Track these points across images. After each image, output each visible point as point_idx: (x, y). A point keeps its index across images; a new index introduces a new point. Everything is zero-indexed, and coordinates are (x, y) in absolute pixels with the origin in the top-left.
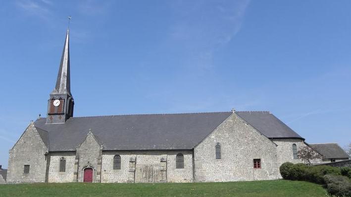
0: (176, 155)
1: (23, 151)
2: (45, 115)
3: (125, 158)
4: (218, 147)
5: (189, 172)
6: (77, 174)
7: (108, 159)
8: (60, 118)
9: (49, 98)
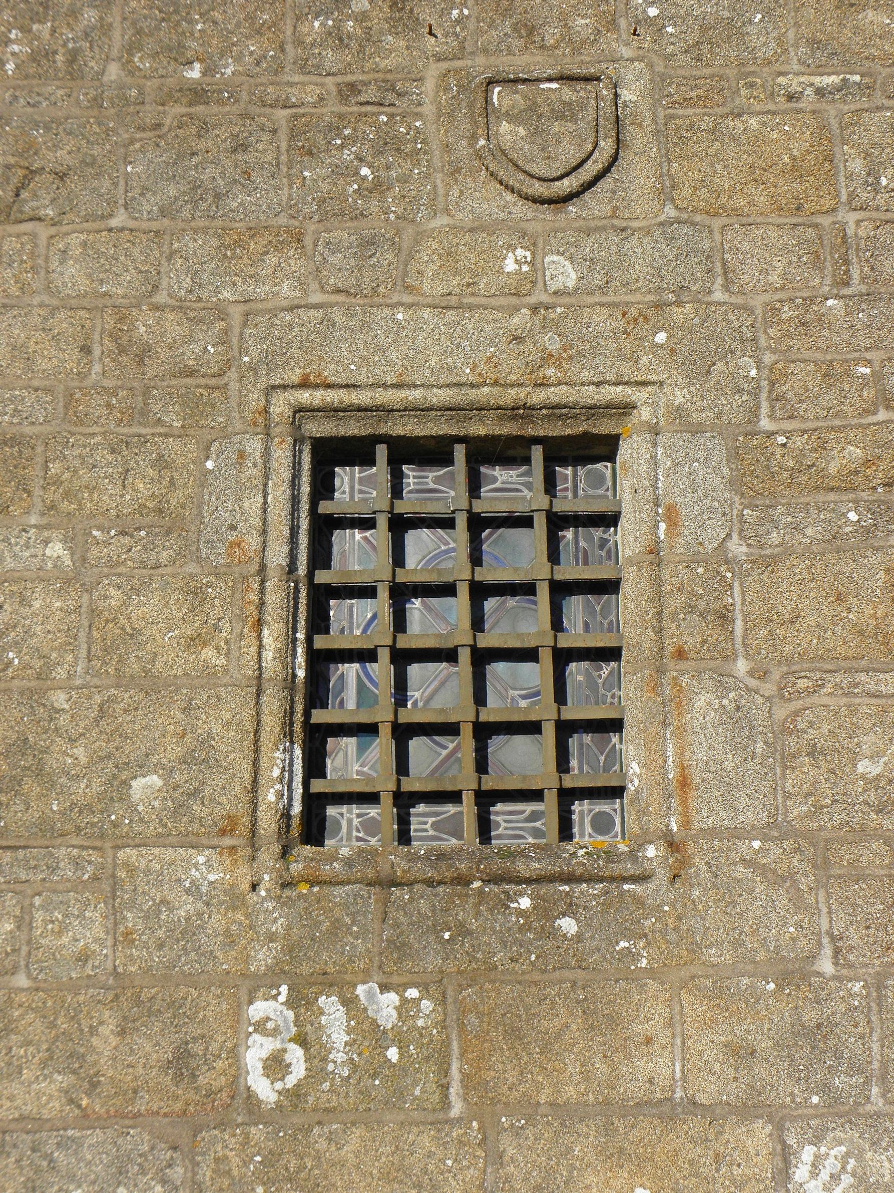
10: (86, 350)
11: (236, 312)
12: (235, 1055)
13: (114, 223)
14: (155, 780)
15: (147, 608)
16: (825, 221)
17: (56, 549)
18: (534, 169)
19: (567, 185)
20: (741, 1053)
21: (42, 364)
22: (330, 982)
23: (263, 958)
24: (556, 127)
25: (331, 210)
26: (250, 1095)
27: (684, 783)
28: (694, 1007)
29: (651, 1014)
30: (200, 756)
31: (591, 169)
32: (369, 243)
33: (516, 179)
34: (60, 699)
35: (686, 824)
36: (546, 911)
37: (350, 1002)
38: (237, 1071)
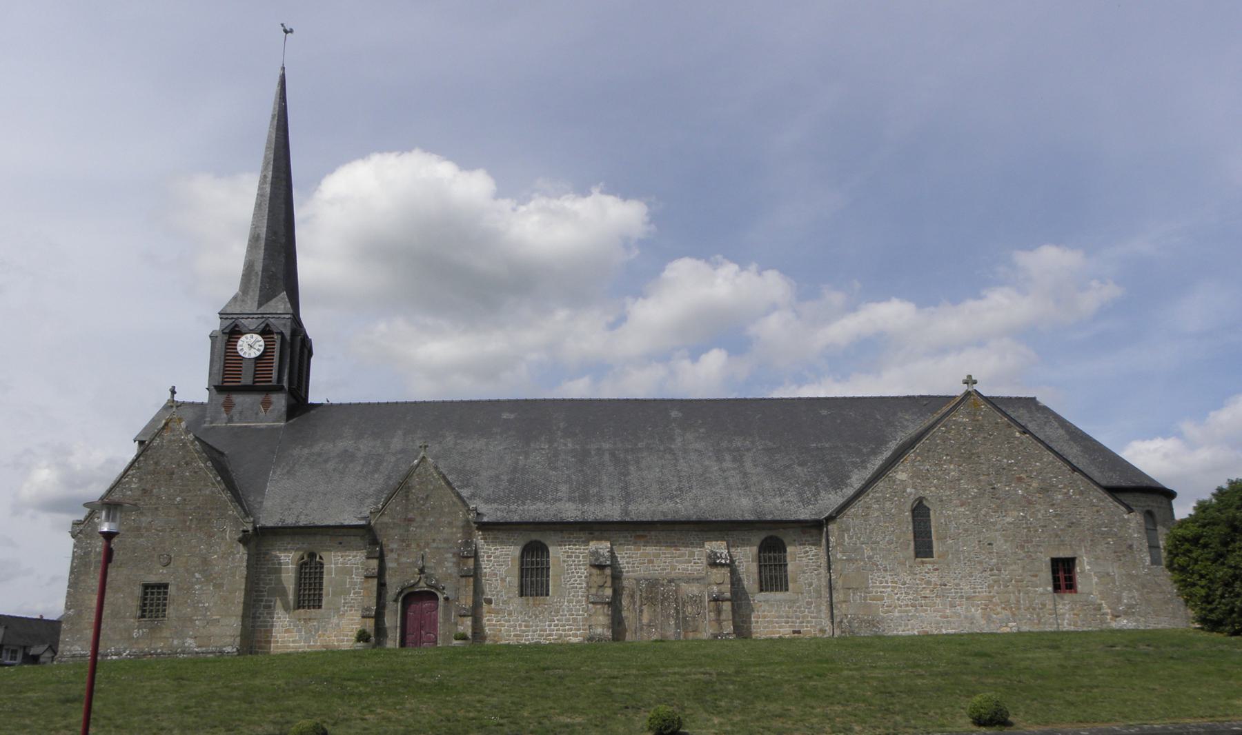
0: (755, 549)
1: (138, 529)
2: (196, 387)
3: (570, 562)
4: (920, 512)
5: (809, 603)
6: (379, 616)
7: (500, 561)
8: (266, 404)
9: (216, 325)
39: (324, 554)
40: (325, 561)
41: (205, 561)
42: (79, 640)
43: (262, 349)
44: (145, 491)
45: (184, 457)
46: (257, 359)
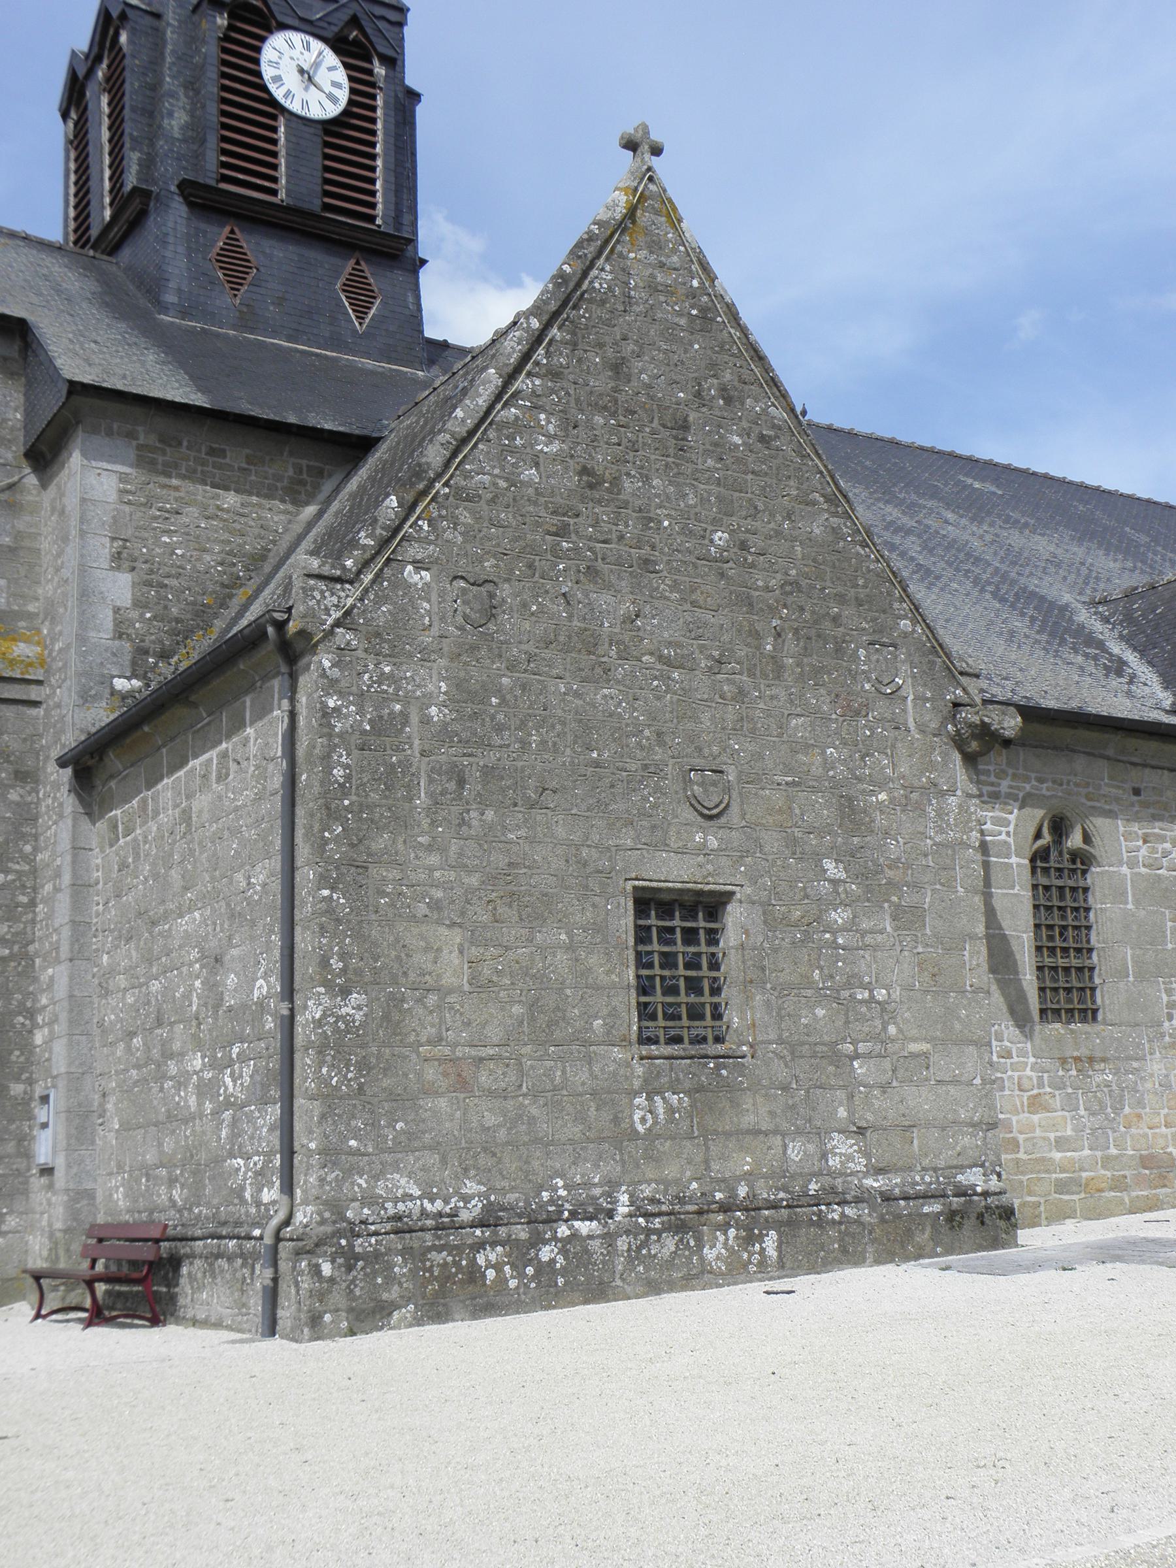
10: (567, 861)
11: (613, 849)
12: (631, 1117)
13: (573, 812)
14: (600, 1022)
15: (593, 960)
16: (789, 830)
17: (563, 937)
18: (705, 804)
19: (715, 812)
20: (772, 1114)
21: (554, 866)
22: (660, 1093)
23: (637, 1084)
24: (712, 789)
25: (642, 814)
26: (636, 1131)
27: (754, 1025)
28: (759, 1100)
29: (747, 1103)
30: (613, 1013)
31: (723, 806)
32: (654, 827)
33: (699, 808)
34: (568, 992)
35: (755, 1039)
36: (718, 1067)
37: (663, 1098)
38: (633, 1123)
39: (1099, 824)
40: (1098, 849)
41: (851, 814)
42: (408, 1143)
43: (343, 96)
44: (590, 478)
45: (714, 368)
46: (329, 127)
